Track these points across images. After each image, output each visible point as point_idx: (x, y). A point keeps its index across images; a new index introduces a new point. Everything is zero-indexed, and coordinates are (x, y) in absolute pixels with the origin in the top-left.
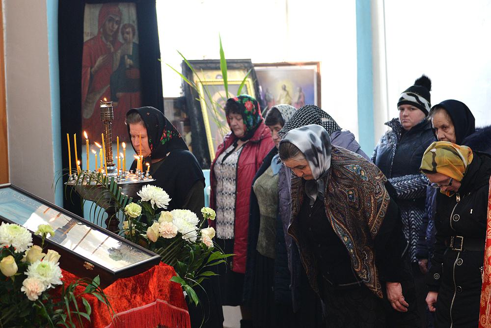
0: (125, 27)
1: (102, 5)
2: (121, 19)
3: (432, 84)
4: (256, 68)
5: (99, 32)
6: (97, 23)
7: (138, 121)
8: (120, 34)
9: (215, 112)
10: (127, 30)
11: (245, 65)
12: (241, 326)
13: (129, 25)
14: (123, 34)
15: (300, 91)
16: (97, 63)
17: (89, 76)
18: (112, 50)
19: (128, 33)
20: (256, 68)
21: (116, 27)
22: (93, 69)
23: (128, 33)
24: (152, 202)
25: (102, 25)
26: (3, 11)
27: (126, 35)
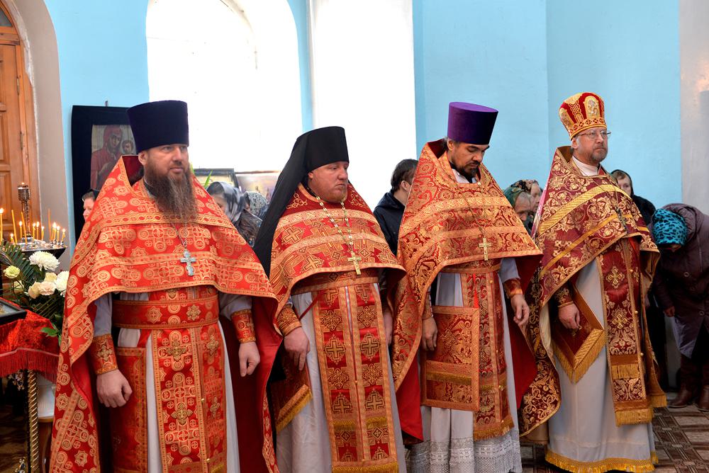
0: (125, 142)
1: (106, 126)
2: (122, 136)
3: (408, 158)
4: (237, 175)
5: (104, 145)
6: (102, 139)
7: (91, 196)
8: (121, 148)
9: (403, 296)
10: (127, 145)
11: (229, 173)
12: (101, 471)
13: (128, 141)
14: (123, 148)
15: (268, 190)
16: (104, 168)
17: (96, 177)
18: (115, 159)
19: (128, 147)
20: (237, 175)
21: (118, 142)
22: (100, 173)
23: (128, 147)
24: (40, 265)
25: (106, 141)
26: (36, 131)
27: (126, 148)
